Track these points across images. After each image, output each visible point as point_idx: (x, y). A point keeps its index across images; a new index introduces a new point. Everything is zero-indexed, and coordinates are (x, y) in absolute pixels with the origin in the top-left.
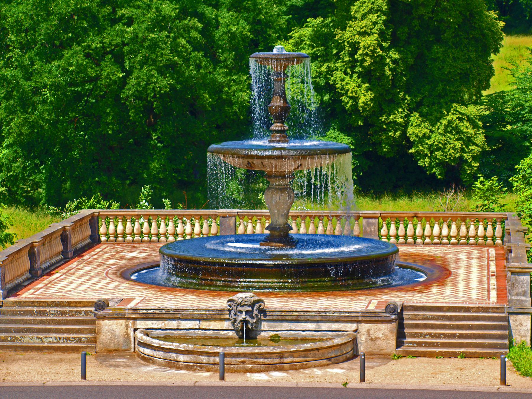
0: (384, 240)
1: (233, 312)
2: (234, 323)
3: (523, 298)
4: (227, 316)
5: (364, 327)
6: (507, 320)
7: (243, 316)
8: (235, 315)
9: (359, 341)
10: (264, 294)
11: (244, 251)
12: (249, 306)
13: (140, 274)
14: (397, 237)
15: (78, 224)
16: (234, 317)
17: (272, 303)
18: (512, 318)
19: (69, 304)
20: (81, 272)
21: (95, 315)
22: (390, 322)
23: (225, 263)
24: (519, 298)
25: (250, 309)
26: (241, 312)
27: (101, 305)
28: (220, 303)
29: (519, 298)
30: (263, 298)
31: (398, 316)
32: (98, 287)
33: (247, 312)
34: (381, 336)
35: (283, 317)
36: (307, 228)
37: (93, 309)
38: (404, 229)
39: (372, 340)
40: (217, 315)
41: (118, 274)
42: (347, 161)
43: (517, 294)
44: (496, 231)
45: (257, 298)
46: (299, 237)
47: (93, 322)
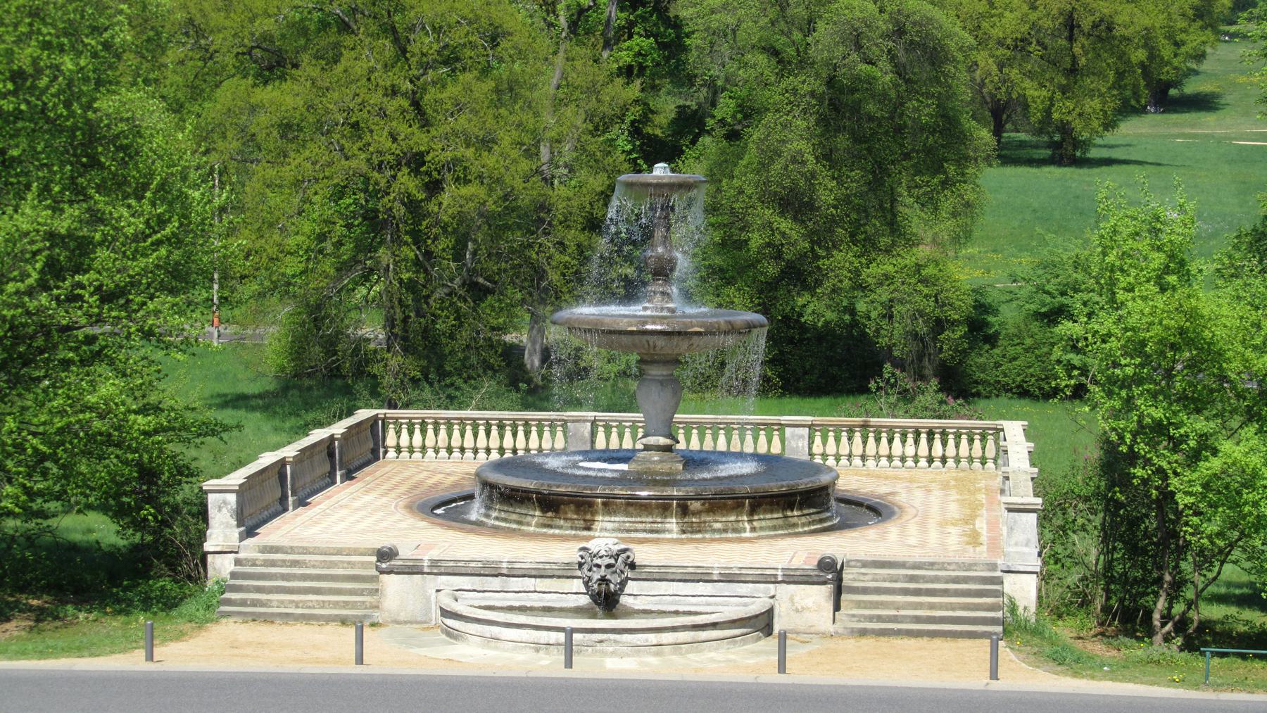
0: (818, 460)
1: (586, 567)
2: (586, 584)
3: (1026, 550)
4: (579, 573)
5: (785, 591)
6: (1000, 581)
7: (603, 572)
8: (590, 570)
9: (776, 612)
10: (633, 541)
11: (609, 475)
12: (611, 557)
13: (446, 507)
14: (838, 458)
15: (354, 431)
16: (589, 574)
17: (644, 554)
18: (1008, 578)
19: (339, 552)
20: (357, 504)
21: (377, 567)
22: (824, 583)
23: (1235, 595)
24: (1019, 549)
25: (612, 561)
26: (599, 566)
27: (385, 555)
28: (563, 551)
29: (1019, 549)
30: (630, 546)
31: (831, 573)
32: (385, 524)
33: (609, 566)
34: (810, 605)
35: (662, 575)
36: (702, 440)
37: (374, 559)
38: (861, 446)
39: (797, 611)
40: (564, 572)
41: (415, 507)
42: (760, 341)
43: (1016, 544)
44: (440, 438)
45: (623, 546)
46: (704, 456)
47: (373, 579)
